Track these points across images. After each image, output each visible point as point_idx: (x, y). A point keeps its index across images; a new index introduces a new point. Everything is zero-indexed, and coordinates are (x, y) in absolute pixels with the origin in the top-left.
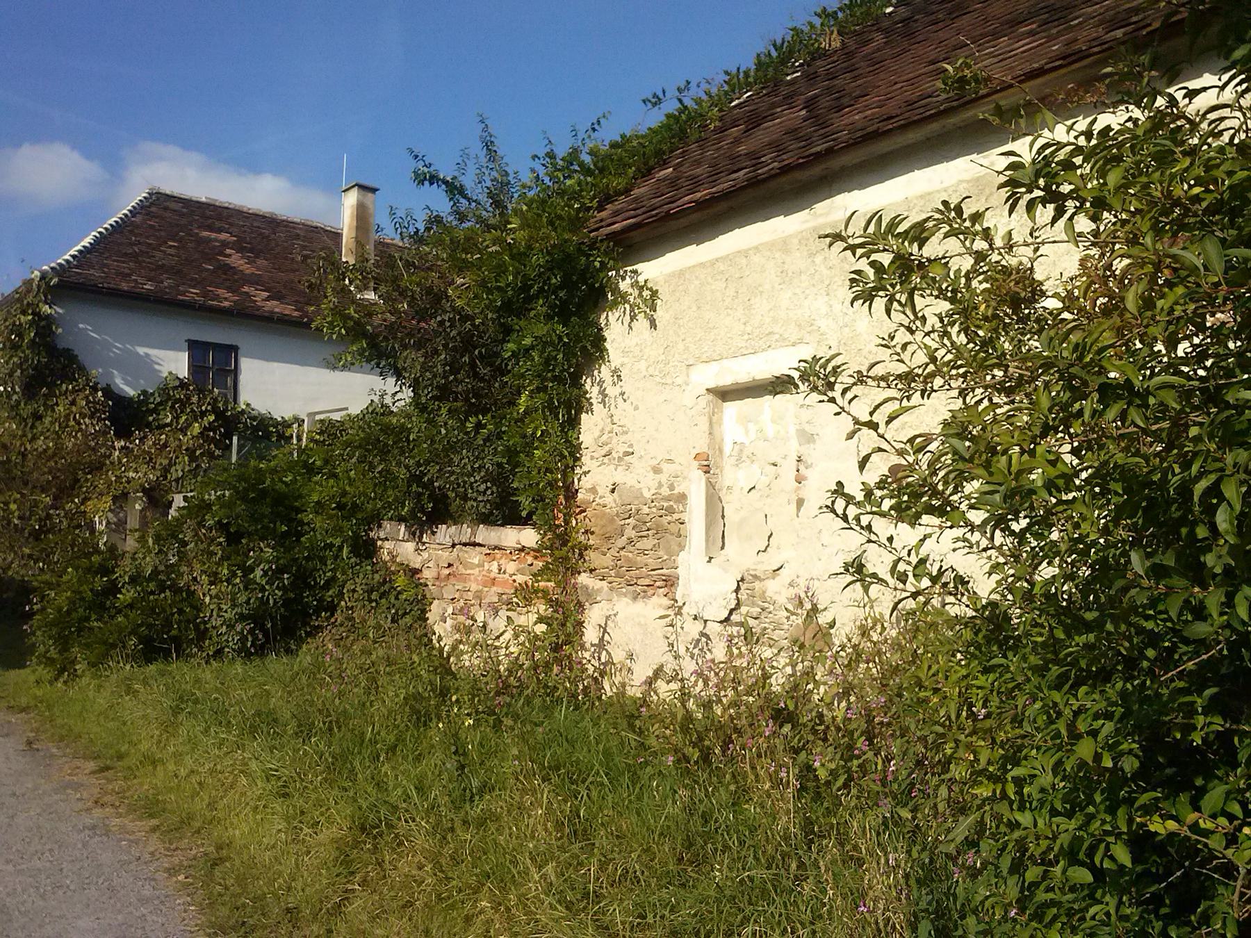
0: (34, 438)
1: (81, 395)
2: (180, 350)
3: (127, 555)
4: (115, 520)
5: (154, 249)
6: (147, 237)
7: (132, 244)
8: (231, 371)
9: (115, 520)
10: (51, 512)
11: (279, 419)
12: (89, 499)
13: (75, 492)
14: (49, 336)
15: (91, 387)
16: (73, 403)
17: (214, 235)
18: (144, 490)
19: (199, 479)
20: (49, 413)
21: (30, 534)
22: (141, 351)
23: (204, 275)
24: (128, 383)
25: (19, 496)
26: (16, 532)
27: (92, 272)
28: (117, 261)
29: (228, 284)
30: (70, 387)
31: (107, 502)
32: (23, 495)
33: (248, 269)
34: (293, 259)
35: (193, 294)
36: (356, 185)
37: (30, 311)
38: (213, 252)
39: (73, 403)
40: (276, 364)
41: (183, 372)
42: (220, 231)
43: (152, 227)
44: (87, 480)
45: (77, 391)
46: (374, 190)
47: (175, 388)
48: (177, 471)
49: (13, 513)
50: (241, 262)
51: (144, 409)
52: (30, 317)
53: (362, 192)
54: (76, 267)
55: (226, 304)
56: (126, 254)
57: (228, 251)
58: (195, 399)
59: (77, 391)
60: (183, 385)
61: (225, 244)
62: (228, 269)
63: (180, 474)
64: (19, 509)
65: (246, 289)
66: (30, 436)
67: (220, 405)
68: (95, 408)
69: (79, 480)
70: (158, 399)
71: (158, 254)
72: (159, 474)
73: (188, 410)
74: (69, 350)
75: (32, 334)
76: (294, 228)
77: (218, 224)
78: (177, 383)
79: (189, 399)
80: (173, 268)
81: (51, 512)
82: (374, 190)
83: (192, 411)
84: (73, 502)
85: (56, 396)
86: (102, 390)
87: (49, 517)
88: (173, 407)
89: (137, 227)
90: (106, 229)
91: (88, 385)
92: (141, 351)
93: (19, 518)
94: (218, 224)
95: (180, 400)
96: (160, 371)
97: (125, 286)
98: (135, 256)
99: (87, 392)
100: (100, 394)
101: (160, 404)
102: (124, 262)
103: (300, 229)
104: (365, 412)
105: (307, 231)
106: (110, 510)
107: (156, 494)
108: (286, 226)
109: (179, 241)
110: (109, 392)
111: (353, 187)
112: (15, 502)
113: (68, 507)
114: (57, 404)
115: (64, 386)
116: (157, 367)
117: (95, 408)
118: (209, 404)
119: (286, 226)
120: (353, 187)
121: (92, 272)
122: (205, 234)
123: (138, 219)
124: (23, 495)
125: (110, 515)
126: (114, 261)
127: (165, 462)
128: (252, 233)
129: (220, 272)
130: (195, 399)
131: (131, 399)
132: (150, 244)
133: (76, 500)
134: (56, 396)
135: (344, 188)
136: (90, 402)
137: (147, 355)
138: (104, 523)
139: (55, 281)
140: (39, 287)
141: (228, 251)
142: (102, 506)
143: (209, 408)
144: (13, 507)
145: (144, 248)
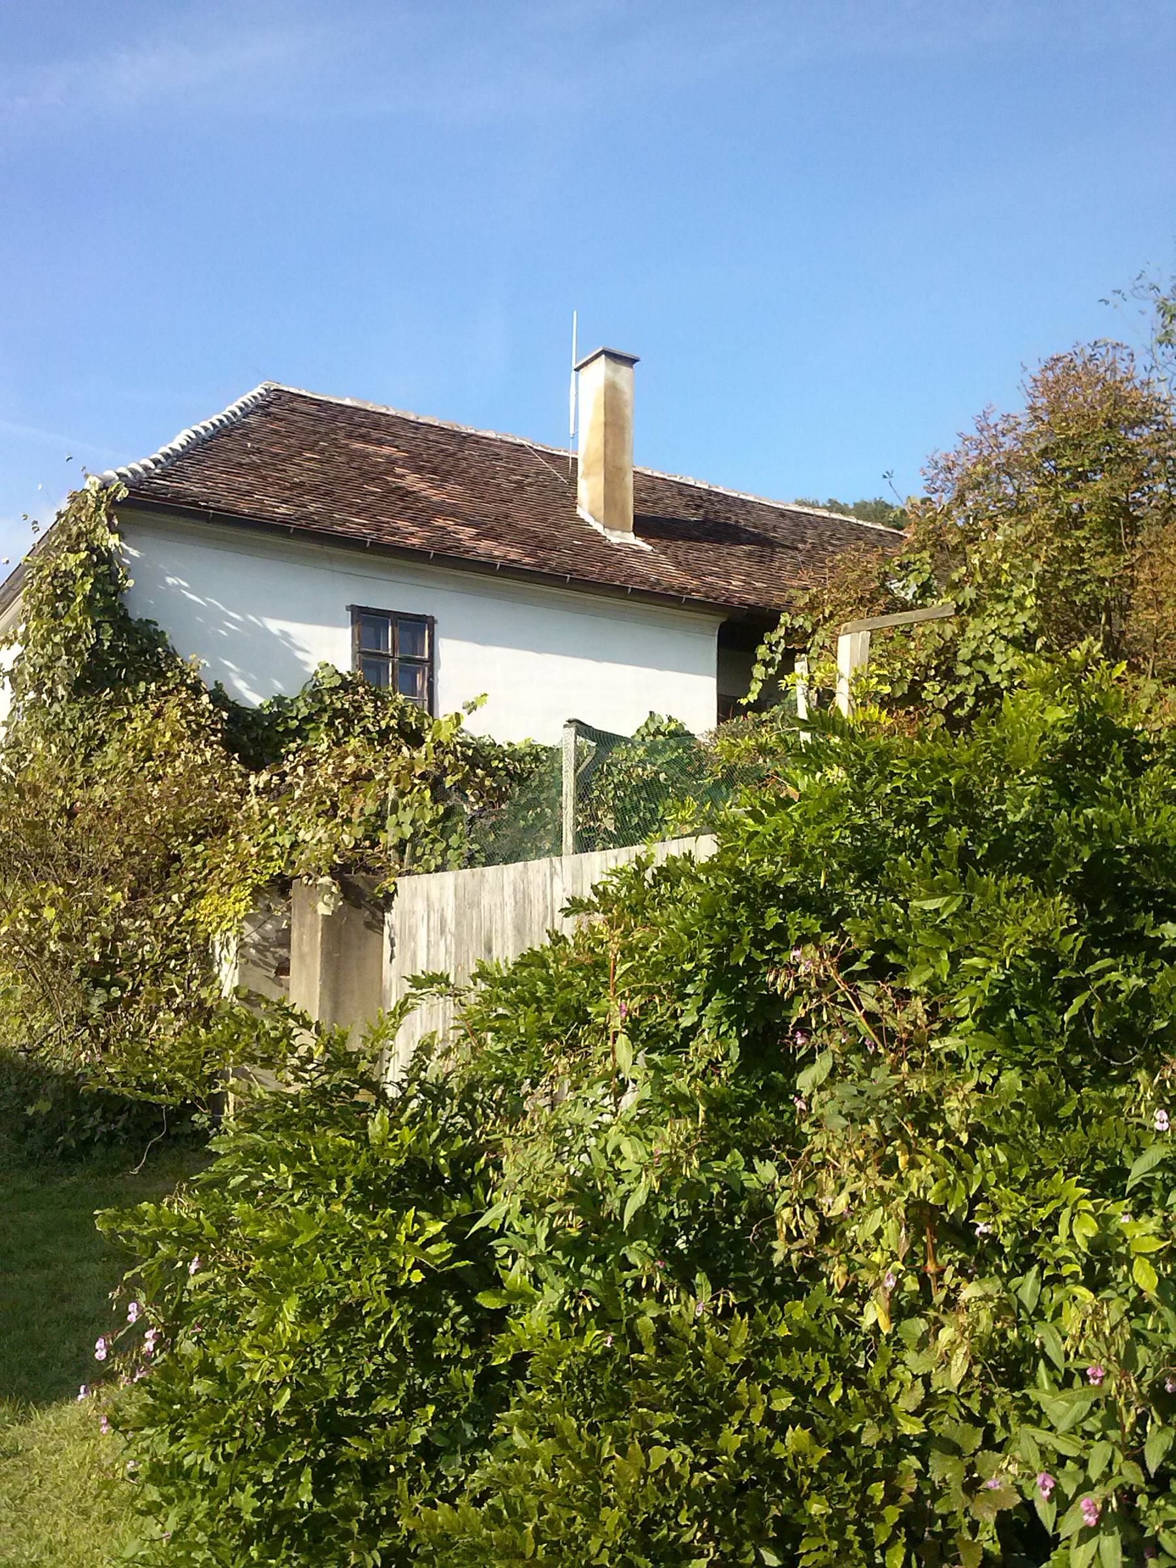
0: (89, 783)
1: (174, 700)
2: (334, 623)
3: (649, 1150)
4: (256, 937)
5: (284, 460)
6: (272, 445)
7: (248, 453)
8: (423, 661)
9: (256, 937)
10: (125, 923)
11: (506, 747)
12: (203, 895)
13: (171, 882)
14: (115, 594)
15: (189, 687)
16: (158, 715)
17: (371, 448)
18: (337, 872)
19: (454, 840)
20: (116, 734)
21: (83, 973)
22: (274, 626)
23: (370, 499)
24: (254, 689)
25: (61, 890)
26: (54, 967)
27: (187, 485)
28: (228, 473)
29: (410, 513)
30: (153, 686)
31: (238, 903)
32: (69, 888)
33: (436, 496)
34: (499, 485)
35: (356, 524)
36: (604, 352)
37: (83, 546)
38: (376, 473)
39: (158, 715)
40: (497, 650)
41: (345, 663)
42: (380, 443)
43: (276, 432)
44: (194, 856)
45: (164, 694)
46: (631, 361)
47: (333, 690)
48: (399, 824)
49: (47, 928)
50: (422, 485)
51: (280, 729)
52: (83, 555)
53: (612, 365)
54: (163, 477)
55: (415, 541)
56: (241, 465)
57: (398, 470)
58: (368, 709)
59: (164, 694)
60: (346, 686)
61: (392, 461)
62: (405, 494)
63: (408, 831)
64: (60, 916)
65: (440, 522)
66: (80, 778)
67: (412, 719)
68: (198, 724)
69: (177, 858)
70: (305, 712)
71: (292, 469)
72: (360, 832)
73: (358, 729)
74: (149, 622)
75: (88, 587)
76: (490, 445)
77: (375, 434)
78: (337, 682)
79: (359, 709)
80: (317, 487)
81: (125, 923)
82: (631, 361)
83: (366, 731)
84: (168, 900)
85: (127, 703)
86: (210, 693)
87: (121, 934)
88: (330, 724)
89: (253, 430)
90: (206, 429)
91: (183, 683)
92: (274, 626)
93: (63, 938)
94: (375, 434)
95: (342, 713)
96: (306, 664)
97: (244, 508)
98: (254, 467)
99: (184, 695)
100: (205, 699)
101: (308, 719)
102: (238, 475)
103: (499, 447)
104: (644, 731)
105: (508, 449)
106: (247, 918)
107: (358, 878)
108: (477, 442)
109: (322, 452)
110: (219, 697)
111: (597, 356)
112: (52, 905)
113: (157, 912)
114: (130, 719)
115: (142, 685)
116: (300, 655)
117: (198, 724)
118: (392, 717)
119: (477, 442)
120: (597, 356)
121: (187, 485)
122: (358, 446)
123: (252, 420)
124: (69, 888)
125: (248, 928)
126: (222, 472)
127: (371, 807)
128: (429, 448)
129: (393, 497)
130: (368, 709)
131: (258, 713)
132: (278, 454)
133: (175, 898)
134: (127, 703)
135: (575, 366)
136: (189, 713)
137: (286, 635)
138: (233, 946)
139: (124, 493)
140: (99, 501)
141: (398, 470)
142: (228, 909)
143: (393, 723)
144: (49, 913)
145: (266, 459)
